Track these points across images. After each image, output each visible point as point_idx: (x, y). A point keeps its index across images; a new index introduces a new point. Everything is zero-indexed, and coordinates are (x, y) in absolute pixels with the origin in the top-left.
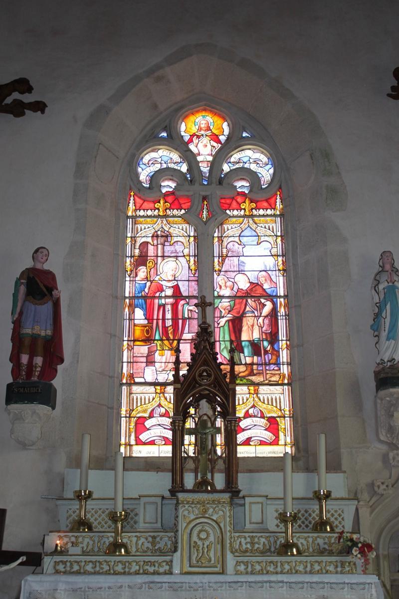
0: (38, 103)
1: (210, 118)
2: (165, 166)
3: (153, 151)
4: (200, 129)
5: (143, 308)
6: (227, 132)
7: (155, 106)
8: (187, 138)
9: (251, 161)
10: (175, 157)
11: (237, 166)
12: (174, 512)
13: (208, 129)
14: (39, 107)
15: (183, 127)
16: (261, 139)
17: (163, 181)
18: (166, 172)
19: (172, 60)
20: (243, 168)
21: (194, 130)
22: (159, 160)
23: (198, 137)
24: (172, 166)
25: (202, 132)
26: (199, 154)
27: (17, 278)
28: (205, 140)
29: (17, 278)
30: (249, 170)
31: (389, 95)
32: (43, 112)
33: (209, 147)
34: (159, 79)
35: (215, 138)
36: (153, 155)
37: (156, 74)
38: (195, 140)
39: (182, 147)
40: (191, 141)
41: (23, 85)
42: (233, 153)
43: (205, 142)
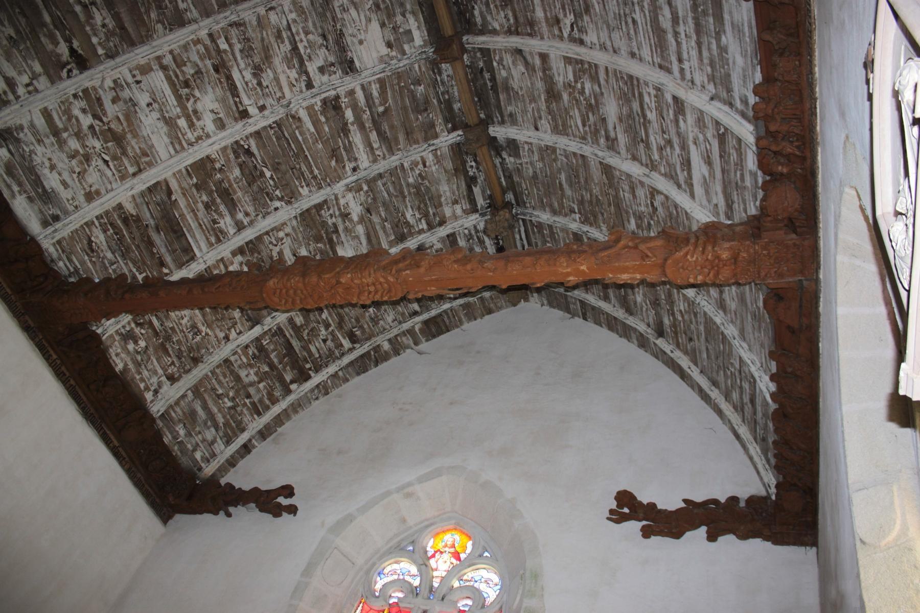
0: (291, 506)
1: (457, 537)
2: (401, 577)
3: (396, 562)
4: (446, 546)
5: (764, 440)
6: (469, 550)
7: (404, 521)
8: (430, 554)
9: (483, 580)
10: (414, 570)
11: (467, 584)
12: (866, 87)
13: (453, 546)
14: (292, 510)
15: (431, 543)
16: (494, 562)
17: (394, 592)
18: (401, 584)
19: (421, 480)
20: (473, 586)
21: (440, 546)
22: (398, 572)
23: (442, 553)
24: (408, 578)
25: (447, 549)
26: (436, 570)
27: (647, 533)
28: (447, 557)
29: (647, 533)
30: (478, 590)
31: (608, 518)
32: (295, 514)
33: (448, 563)
34: (409, 495)
35: (456, 556)
36: (395, 566)
37: (406, 491)
38: (437, 555)
39: (423, 562)
40: (433, 556)
41: (288, 491)
42: (466, 571)
43: (445, 559)
